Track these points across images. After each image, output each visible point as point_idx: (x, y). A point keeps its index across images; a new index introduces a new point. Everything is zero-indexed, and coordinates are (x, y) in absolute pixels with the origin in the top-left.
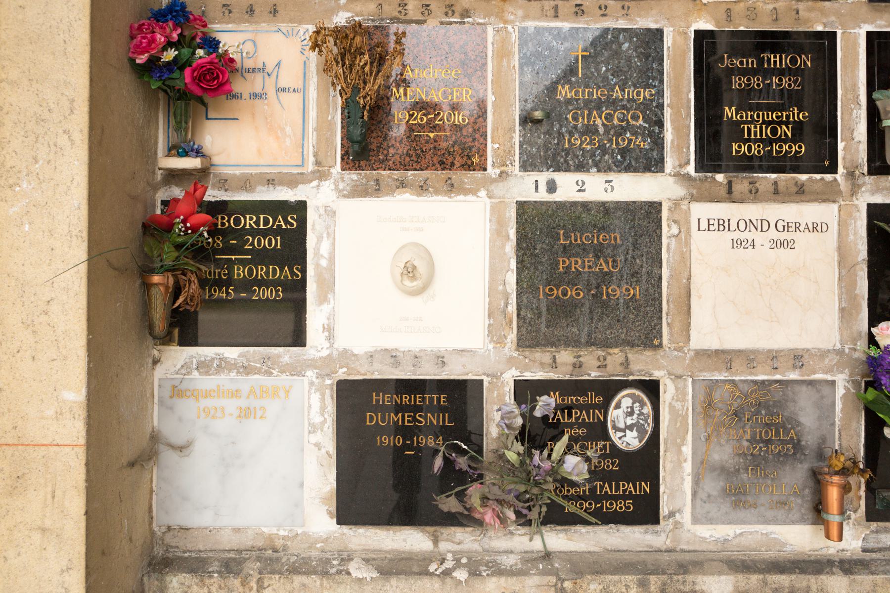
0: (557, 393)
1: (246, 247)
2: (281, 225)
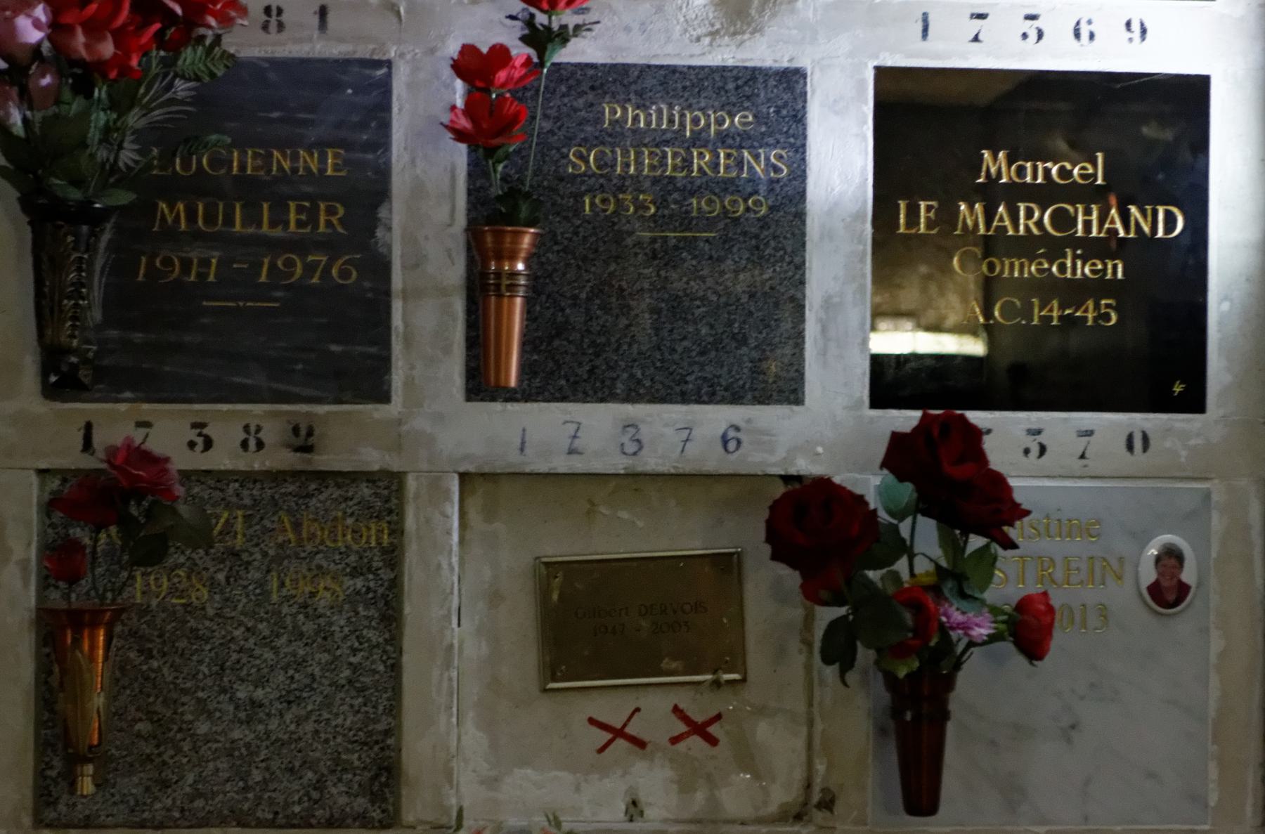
0: (1001, 154)
1: (95, 348)
2: (1005, 228)
